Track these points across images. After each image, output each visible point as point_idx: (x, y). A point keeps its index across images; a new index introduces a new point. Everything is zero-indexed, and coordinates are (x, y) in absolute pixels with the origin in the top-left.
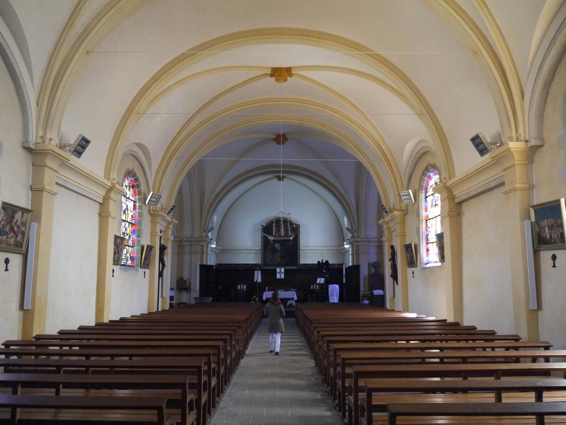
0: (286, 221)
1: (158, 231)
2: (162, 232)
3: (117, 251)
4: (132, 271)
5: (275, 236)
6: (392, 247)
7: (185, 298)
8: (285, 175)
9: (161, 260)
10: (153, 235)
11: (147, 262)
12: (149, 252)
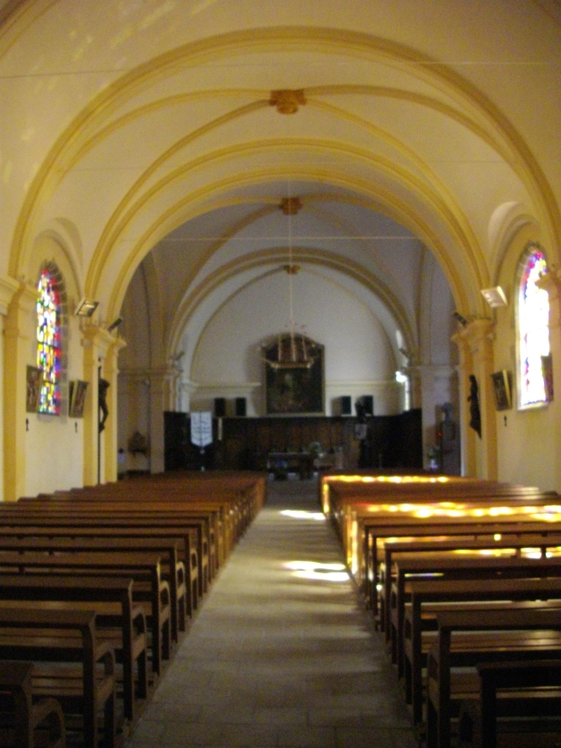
0: (298, 339)
1: (95, 358)
2: (102, 361)
3: (31, 390)
4: (56, 422)
5: (282, 362)
6: (473, 379)
7: (141, 464)
8: (299, 264)
9: (102, 404)
10: (88, 364)
11: (79, 408)
12: (82, 392)
